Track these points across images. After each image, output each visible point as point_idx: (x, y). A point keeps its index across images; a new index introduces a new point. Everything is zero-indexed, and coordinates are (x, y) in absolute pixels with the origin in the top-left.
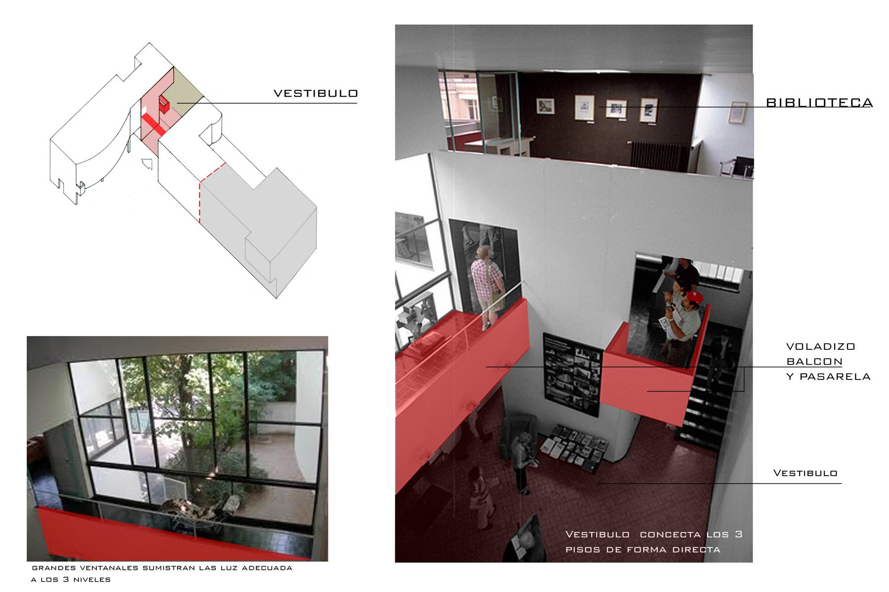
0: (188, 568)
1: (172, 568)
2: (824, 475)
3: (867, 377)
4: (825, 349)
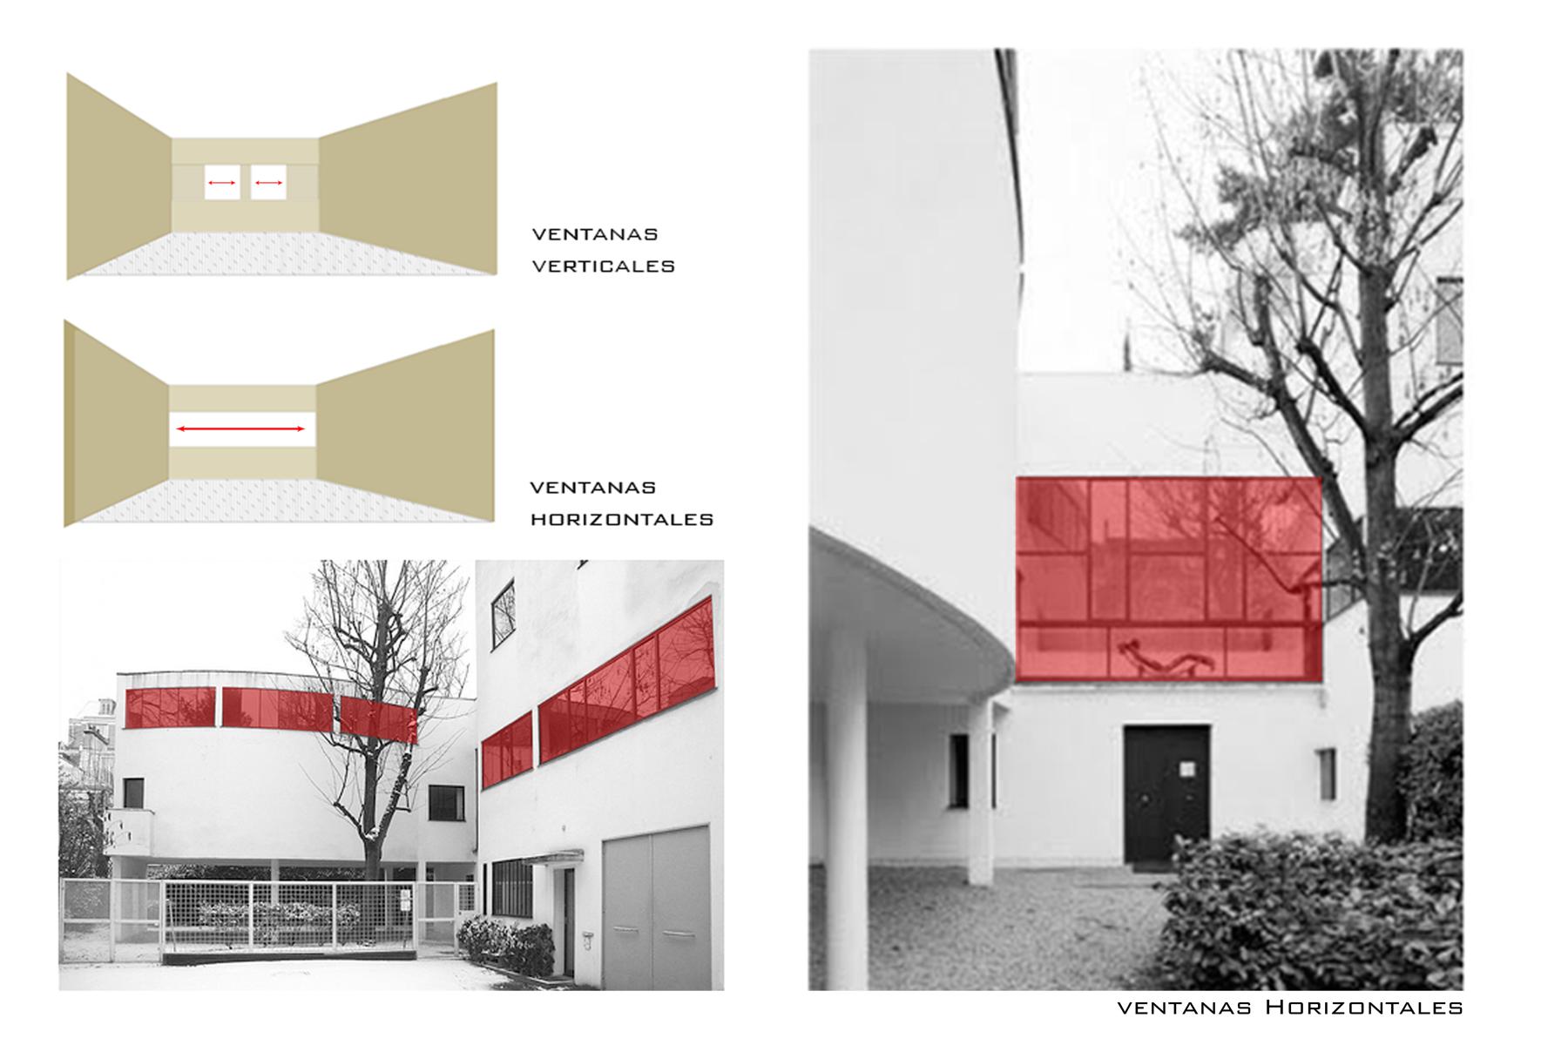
4: (1420, 1013)
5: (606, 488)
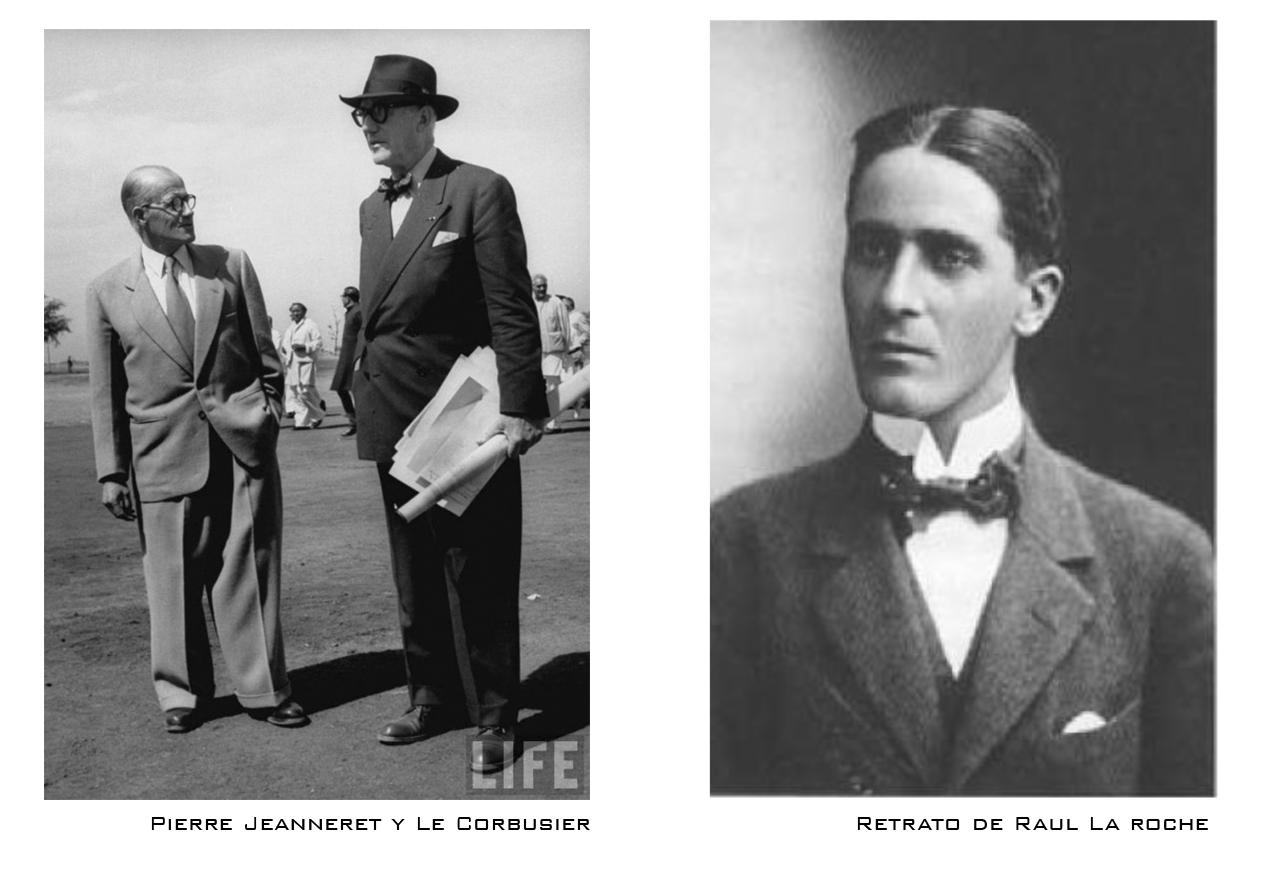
0: (289, 825)
1: (933, 825)
2: (1069, 829)
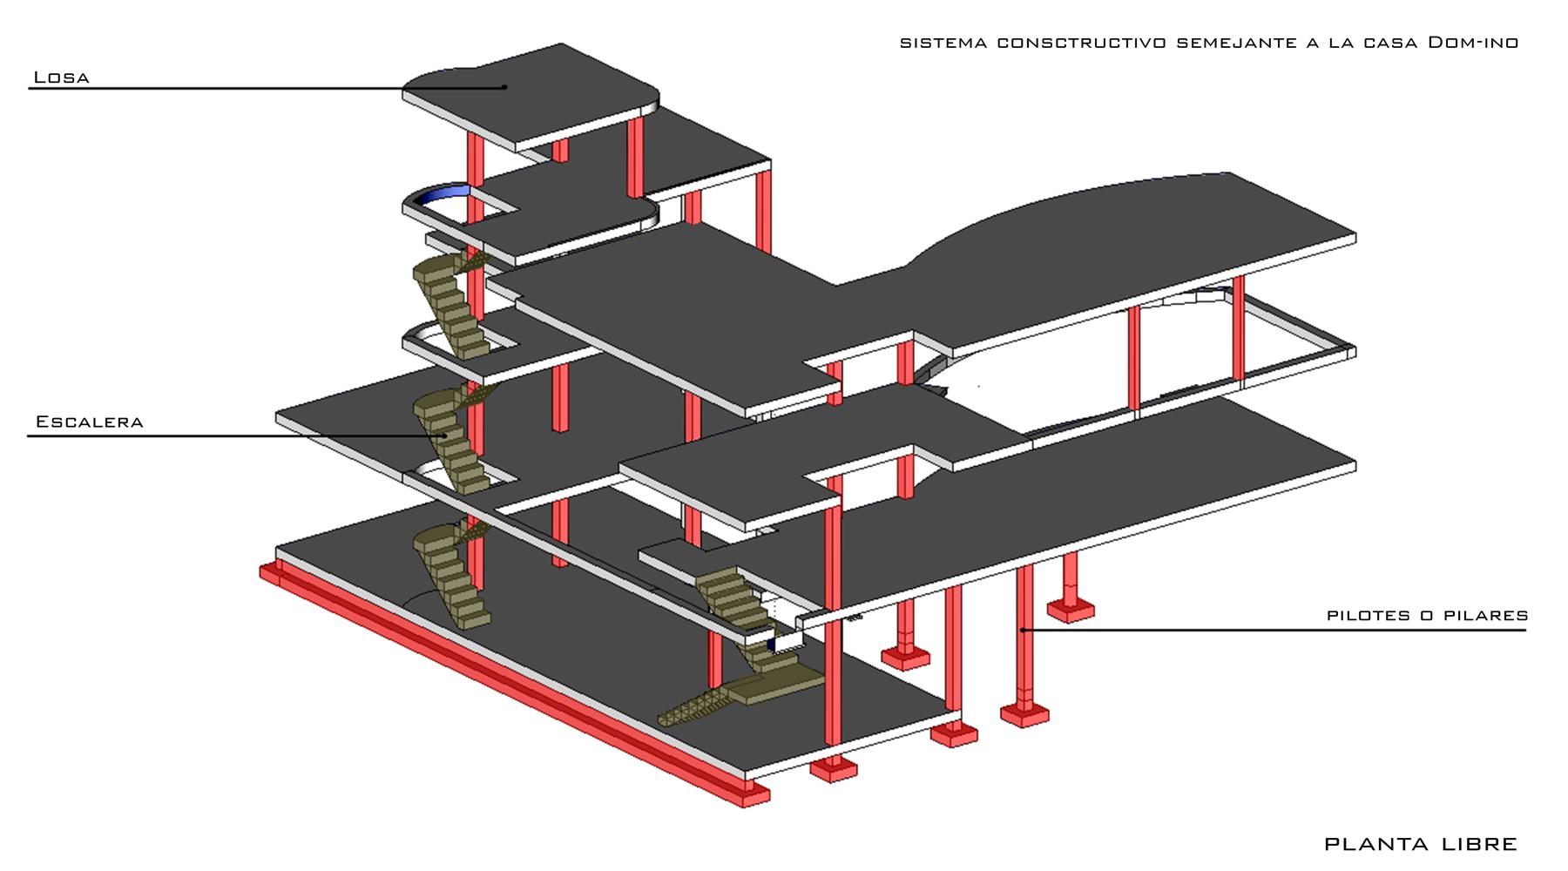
0: (1257, 44)
1: (934, 43)
3: (906, 43)
4: (95, 426)
5: (1376, 844)
